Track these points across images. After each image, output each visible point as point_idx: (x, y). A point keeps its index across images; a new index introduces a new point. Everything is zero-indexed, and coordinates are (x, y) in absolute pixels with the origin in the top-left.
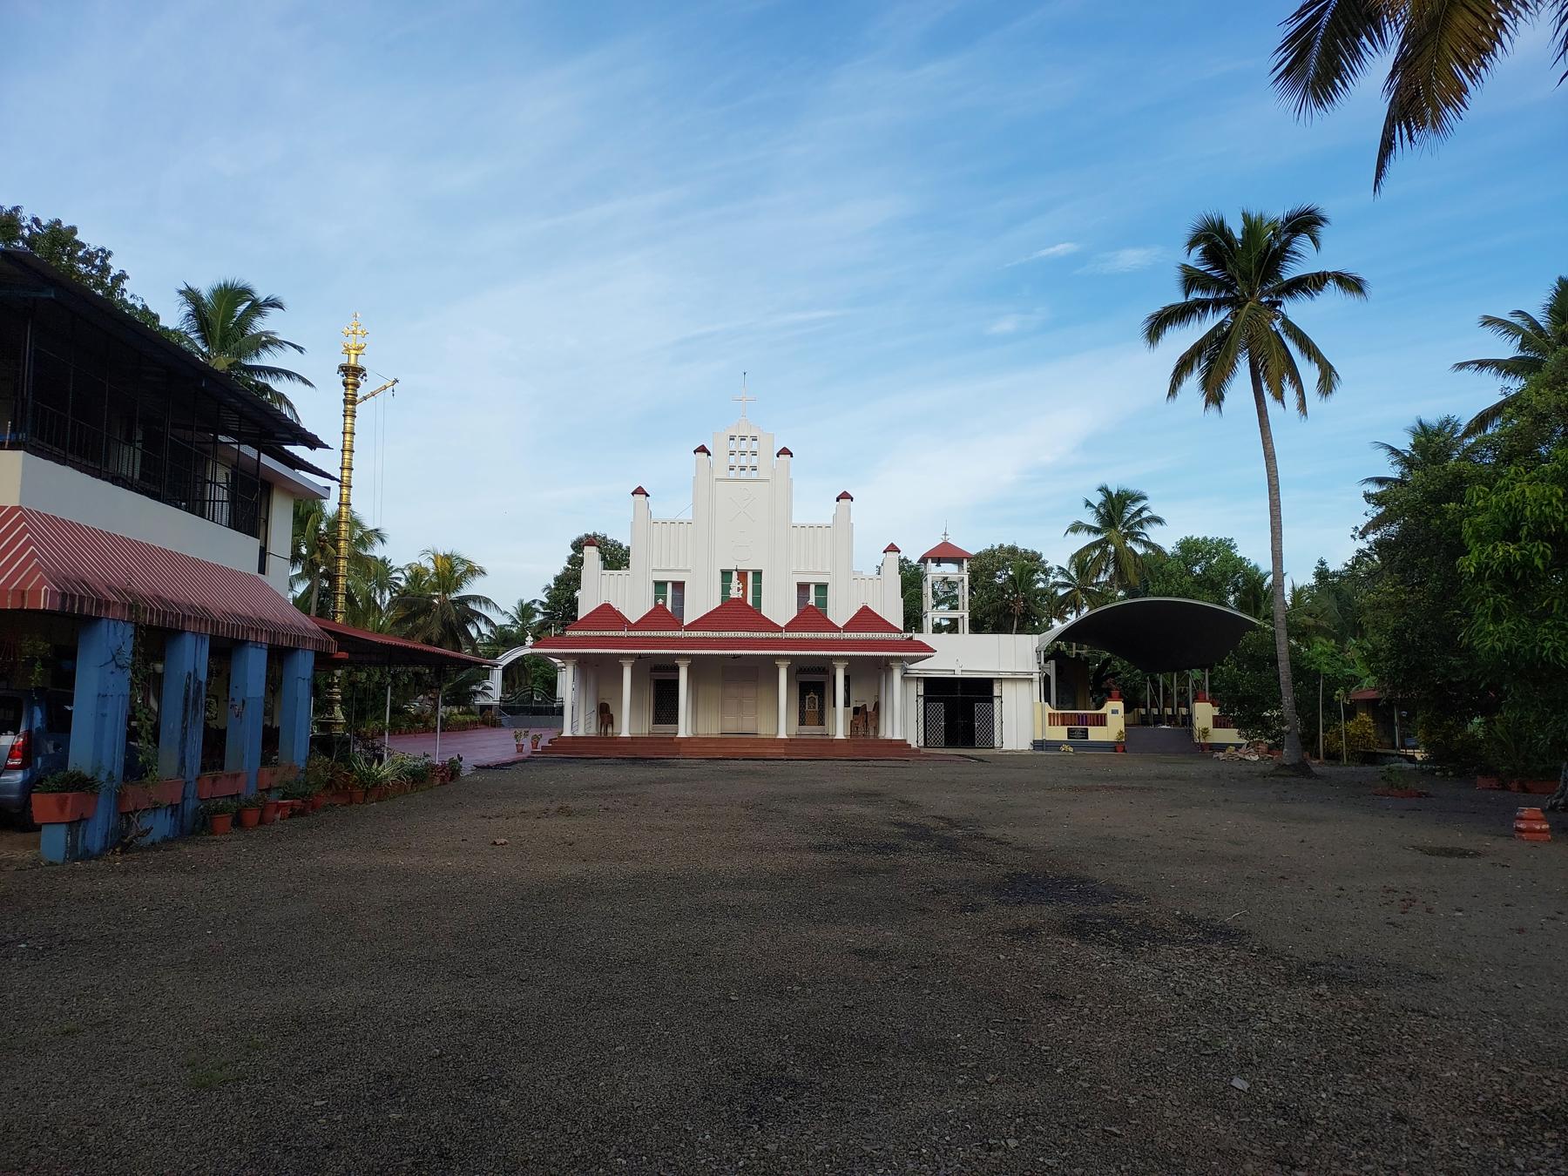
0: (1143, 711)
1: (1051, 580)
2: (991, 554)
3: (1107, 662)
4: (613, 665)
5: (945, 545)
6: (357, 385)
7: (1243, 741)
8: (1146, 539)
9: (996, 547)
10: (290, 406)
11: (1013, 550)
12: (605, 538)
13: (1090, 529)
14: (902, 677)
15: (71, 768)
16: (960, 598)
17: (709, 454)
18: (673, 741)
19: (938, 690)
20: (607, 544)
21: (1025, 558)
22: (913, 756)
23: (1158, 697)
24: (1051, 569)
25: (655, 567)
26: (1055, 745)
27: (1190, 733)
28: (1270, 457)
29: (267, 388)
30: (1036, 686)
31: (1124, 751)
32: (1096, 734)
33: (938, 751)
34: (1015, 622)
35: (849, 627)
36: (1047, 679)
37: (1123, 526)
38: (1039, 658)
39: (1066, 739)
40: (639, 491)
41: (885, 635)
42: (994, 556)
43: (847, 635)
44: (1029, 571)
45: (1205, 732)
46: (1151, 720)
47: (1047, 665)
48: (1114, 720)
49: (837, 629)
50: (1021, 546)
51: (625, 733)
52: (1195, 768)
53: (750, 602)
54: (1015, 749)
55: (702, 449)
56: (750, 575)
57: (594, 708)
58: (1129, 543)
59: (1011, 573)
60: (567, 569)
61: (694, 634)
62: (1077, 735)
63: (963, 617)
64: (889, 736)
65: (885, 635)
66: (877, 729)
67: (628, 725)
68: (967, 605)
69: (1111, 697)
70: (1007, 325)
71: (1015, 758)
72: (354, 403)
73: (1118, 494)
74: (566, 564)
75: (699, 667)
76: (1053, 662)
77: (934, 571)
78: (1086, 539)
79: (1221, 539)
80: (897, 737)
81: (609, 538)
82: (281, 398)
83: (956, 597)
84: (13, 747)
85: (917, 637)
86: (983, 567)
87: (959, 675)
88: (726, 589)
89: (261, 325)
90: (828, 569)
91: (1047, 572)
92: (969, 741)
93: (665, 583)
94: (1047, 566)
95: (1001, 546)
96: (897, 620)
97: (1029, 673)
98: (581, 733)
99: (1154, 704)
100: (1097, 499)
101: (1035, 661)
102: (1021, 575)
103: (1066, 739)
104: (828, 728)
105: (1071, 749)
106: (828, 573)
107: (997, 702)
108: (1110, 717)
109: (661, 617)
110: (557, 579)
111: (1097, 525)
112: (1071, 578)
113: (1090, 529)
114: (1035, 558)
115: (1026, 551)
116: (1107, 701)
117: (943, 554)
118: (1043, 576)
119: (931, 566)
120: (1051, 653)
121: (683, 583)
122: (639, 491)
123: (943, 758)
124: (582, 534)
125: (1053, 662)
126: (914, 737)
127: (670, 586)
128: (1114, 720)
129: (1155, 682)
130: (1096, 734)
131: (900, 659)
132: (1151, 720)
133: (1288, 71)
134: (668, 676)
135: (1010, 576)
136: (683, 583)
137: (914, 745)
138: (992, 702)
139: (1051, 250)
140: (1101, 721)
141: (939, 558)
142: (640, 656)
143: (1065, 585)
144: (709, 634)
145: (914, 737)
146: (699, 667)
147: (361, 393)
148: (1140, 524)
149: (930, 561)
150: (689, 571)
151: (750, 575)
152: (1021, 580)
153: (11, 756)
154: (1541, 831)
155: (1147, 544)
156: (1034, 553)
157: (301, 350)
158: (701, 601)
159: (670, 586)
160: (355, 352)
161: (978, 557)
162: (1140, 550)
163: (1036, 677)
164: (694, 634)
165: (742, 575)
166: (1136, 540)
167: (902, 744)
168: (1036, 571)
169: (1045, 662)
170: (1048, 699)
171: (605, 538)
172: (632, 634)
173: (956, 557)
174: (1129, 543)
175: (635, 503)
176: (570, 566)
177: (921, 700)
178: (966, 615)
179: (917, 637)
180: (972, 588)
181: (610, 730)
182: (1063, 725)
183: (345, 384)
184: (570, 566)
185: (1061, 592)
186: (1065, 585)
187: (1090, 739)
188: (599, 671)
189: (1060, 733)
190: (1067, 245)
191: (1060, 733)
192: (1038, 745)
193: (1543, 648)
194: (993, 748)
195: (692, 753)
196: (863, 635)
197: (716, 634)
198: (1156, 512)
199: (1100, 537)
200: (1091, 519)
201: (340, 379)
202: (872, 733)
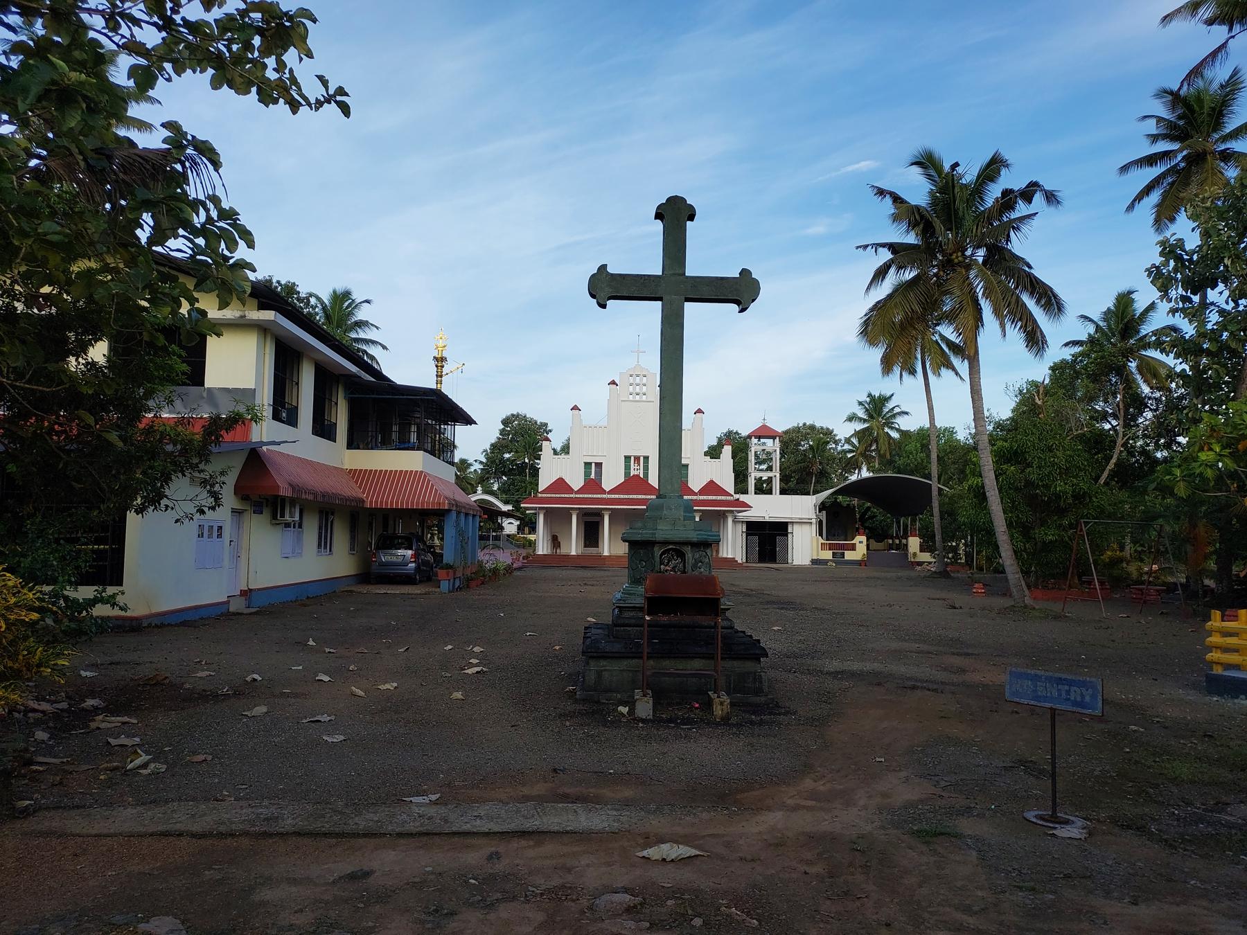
0: (890, 541)
1: (839, 448)
2: (797, 430)
3: (869, 508)
4: (567, 514)
5: (764, 427)
6: (443, 367)
7: (934, 560)
8: (897, 427)
9: (801, 425)
10: (377, 363)
11: (812, 427)
12: (525, 416)
13: (860, 419)
14: (733, 521)
15: (444, 562)
16: (774, 459)
17: (617, 385)
18: (600, 557)
19: (754, 528)
20: (526, 421)
21: (821, 433)
22: (739, 567)
23: (896, 531)
24: (840, 440)
25: (585, 453)
26: (825, 562)
27: (906, 555)
28: (931, 408)
29: (365, 352)
30: (814, 527)
31: (866, 566)
32: (849, 555)
33: (754, 565)
34: (814, 478)
35: (702, 492)
36: (820, 523)
37: (882, 418)
38: (815, 509)
39: (831, 558)
40: (575, 408)
41: (723, 498)
42: (799, 432)
43: (702, 498)
44: (824, 443)
45: (915, 554)
46: (894, 547)
47: (821, 514)
48: (860, 547)
49: (695, 494)
50: (818, 425)
51: (606, 553)
52: (904, 573)
53: (642, 476)
54: (800, 564)
55: (613, 383)
56: (642, 459)
57: (550, 538)
58: (886, 430)
59: (811, 443)
60: (499, 438)
61: (613, 496)
62: (838, 556)
63: (775, 476)
64: (725, 556)
65: (723, 498)
66: (717, 551)
67: (573, 546)
68: (778, 468)
69: (859, 534)
70: (819, 228)
71: (800, 569)
72: (441, 376)
73: (880, 397)
74: (498, 435)
75: (614, 515)
76: (824, 512)
77: (755, 446)
78: (860, 426)
79: (947, 428)
80: (730, 556)
81: (528, 416)
82: (372, 358)
83: (772, 459)
84: (412, 555)
85: (743, 498)
86: (790, 440)
87: (767, 520)
88: (627, 467)
89: (361, 315)
90: (689, 456)
91: (836, 442)
92: (773, 560)
93: (591, 463)
94: (837, 438)
95: (805, 424)
96: (731, 489)
97: (809, 519)
98: (545, 553)
99: (897, 537)
100: (864, 398)
101: (814, 511)
102: (818, 444)
103: (831, 558)
104: (600, 549)
105: (834, 565)
106: (689, 458)
107: (790, 536)
108: (858, 545)
109: (593, 484)
110: (492, 445)
111: (865, 417)
112: (853, 445)
113: (860, 419)
114: (829, 433)
115: (822, 428)
116: (856, 536)
117: (763, 433)
118: (834, 446)
119: (754, 441)
120: (822, 507)
121: (602, 463)
122: (575, 408)
123: (756, 569)
124: (509, 414)
125: (824, 512)
126: (740, 557)
127: (593, 465)
128: (860, 547)
129: (898, 523)
130: (849, 555)
131: (732, 511)
132: (894, 547)
133: (861, 333)
134: (595, 519)
135: (810, 445)
136: (602, 463)
137: (740, 561)
138: (787, 536)
139: (857, 166)
140: (853, 548)
141: (760, 436)
142: (579, 508)
143: (850, 451)
144: (622, 496)
145: (740, 557)
146: (614, 515)
147: (445, 370)
148: (894, 416)
149: (753, 438)
150: (605, 456)
151: (642, 459)
152: (818, 448)
153: (411, 558)
154: (981, 593)
155: (898, 430)
156: (828, 429)
157: (377, 328)
158: (612, 478)
159: (593, 465)
160: (441, 349)
161: (786, 432)
162: (895, 435)
163: (814, 521)
164: (613, 496)
165: (637, 459)
166: (892, 428)
167: (733, 560)
168: (828, 442)
169: (820, 512)
170: (821, 534)
171: (525, 416)
172: (578, 496)
173: (772, 435)
174: (886, 430)
175: (573, 415)
176: (501, 437)
177: (744, 535)
178: (778, 475)
179: (743, 498)
180: (782, 455)
181: (558, 551)
182: (830, 549)
183: (437, 366)
184: (501, 437)
185: (849, 455)
186: (850, 451)
187: (846, 558)
188: (557, 518)
189: (827, 555)
190: (867, 163)
191: (827, 555)
192: (814, 562)
193: (980, 522)
194: (255, 389)
195: (612, 564)
196: (710, 498)
197: (626, 496)
198: (904, 409)
199: (866, 425)
200: (861, 413)
201: (433, 363)
202: (714, 554)
